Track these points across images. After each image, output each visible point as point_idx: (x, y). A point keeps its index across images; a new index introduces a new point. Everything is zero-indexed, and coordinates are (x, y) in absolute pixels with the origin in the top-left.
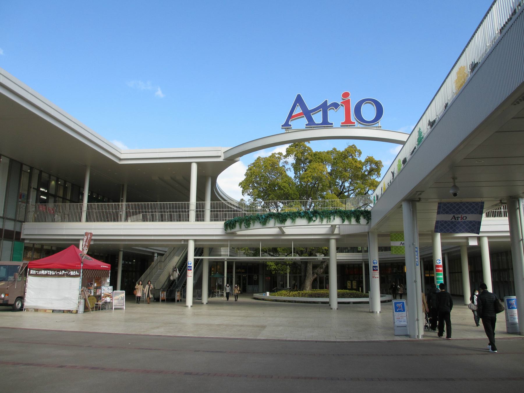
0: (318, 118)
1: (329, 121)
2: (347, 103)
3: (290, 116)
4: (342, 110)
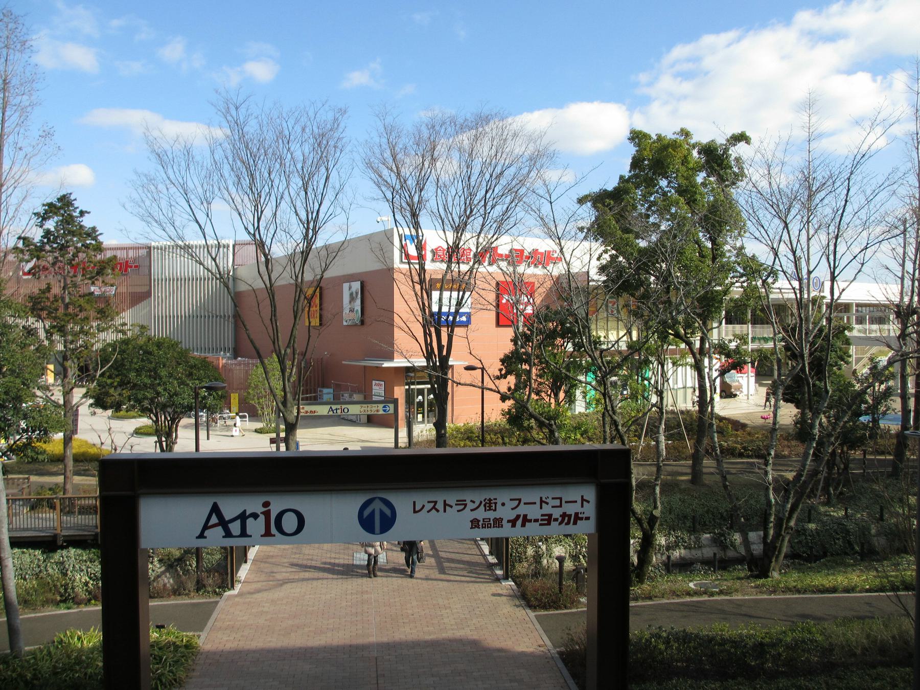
0: (235, 528)
1: (249, 532)
2: (267, 514)
3: (206, 527)
4: (262, 518)
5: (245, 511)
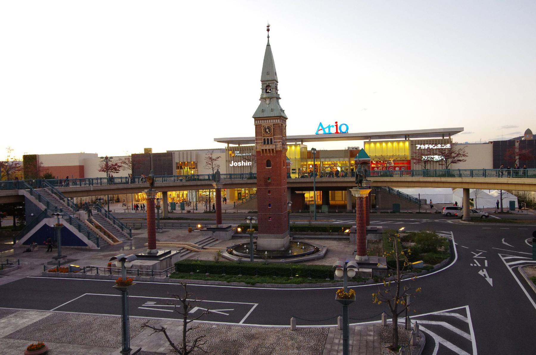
2: (337, 126)
5: (329, 125)
